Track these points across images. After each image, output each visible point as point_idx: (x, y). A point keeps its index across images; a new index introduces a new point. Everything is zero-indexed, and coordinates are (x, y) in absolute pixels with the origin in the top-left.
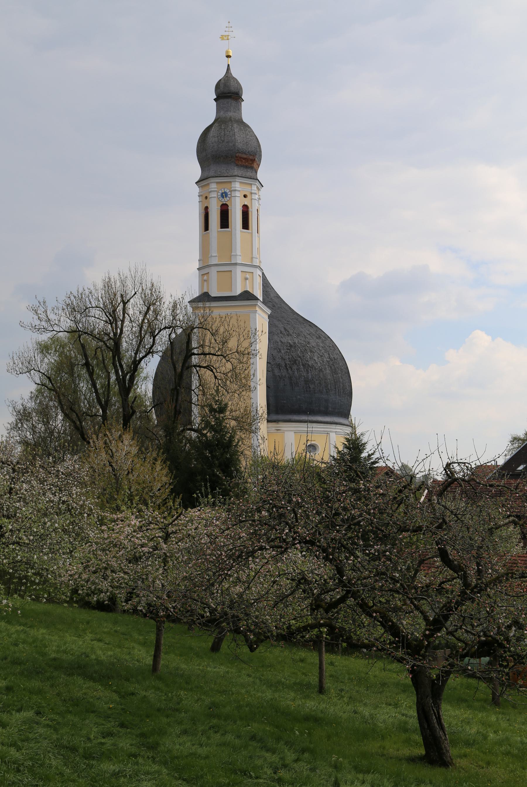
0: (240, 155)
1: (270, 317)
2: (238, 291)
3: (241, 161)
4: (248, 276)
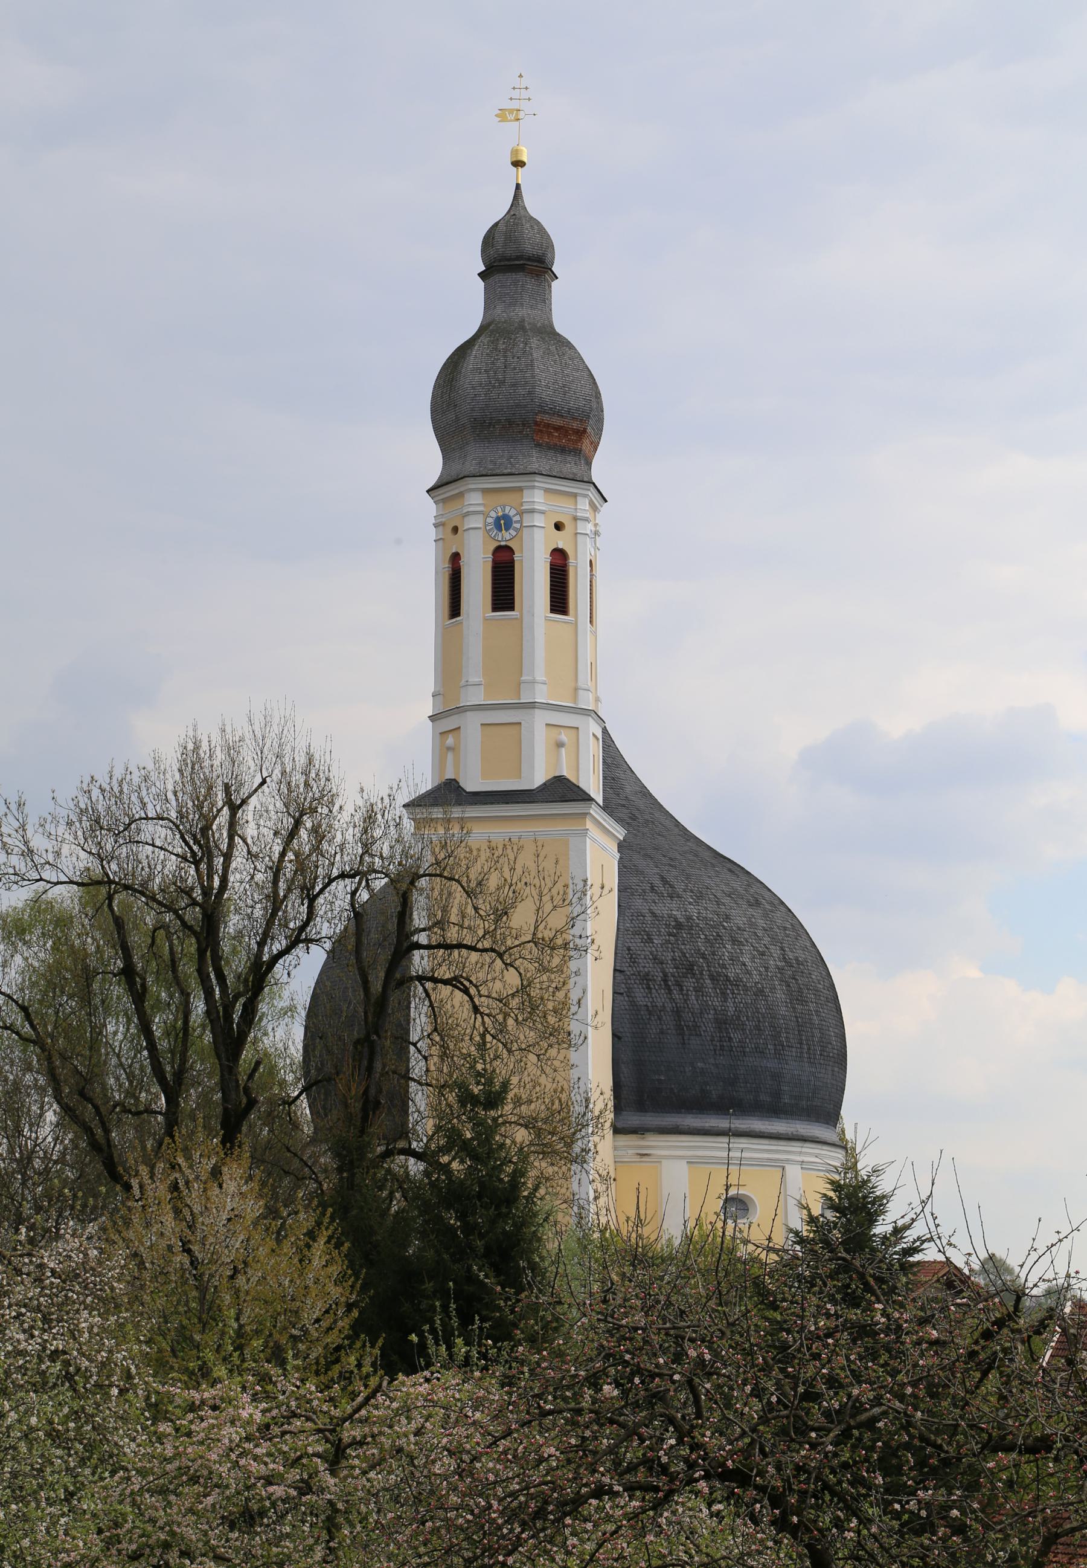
0: (546, 418)
1: (621, 846)
2: (539, 778)
3: (550, 434)
4: (564, 737)
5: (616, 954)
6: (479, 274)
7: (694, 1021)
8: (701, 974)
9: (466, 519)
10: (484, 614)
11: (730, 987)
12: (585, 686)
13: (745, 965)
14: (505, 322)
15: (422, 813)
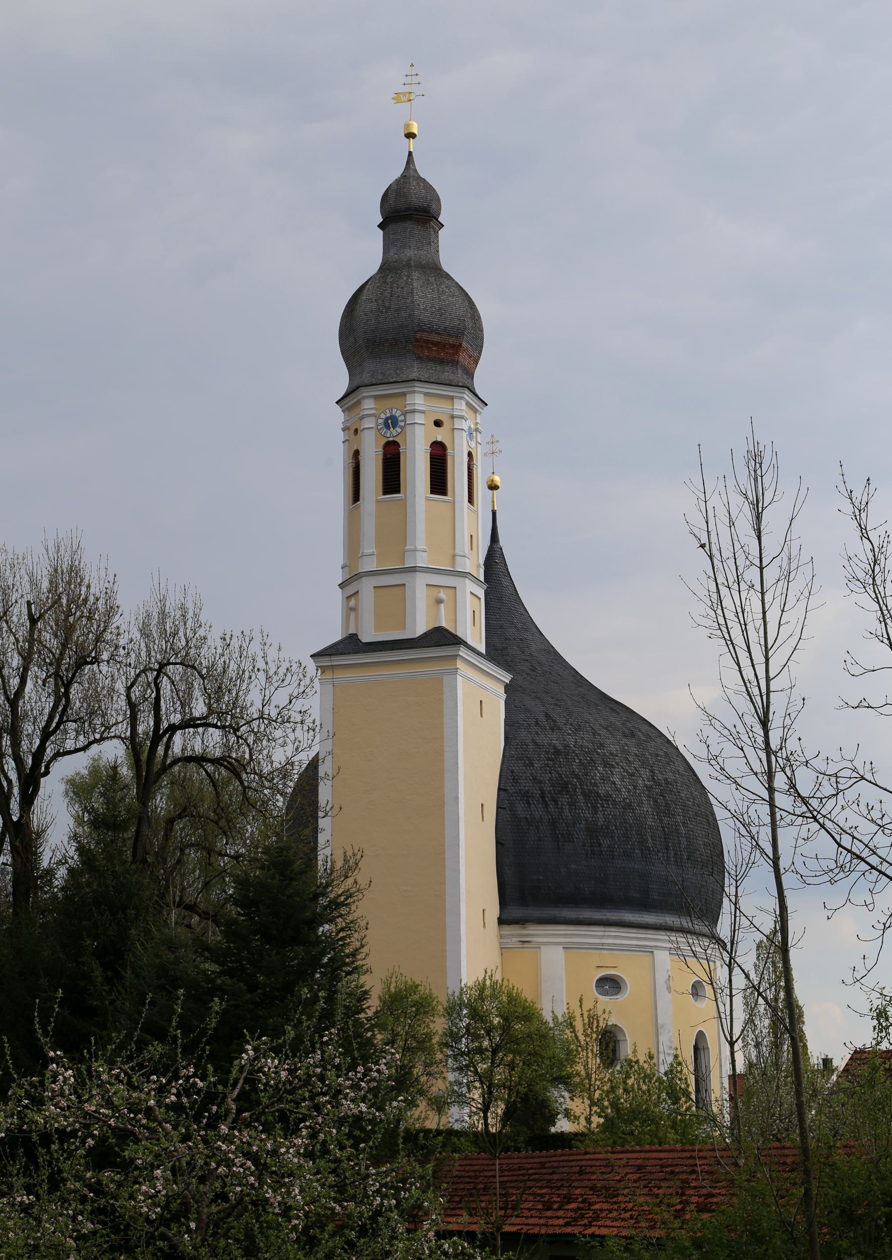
0: (425, 336)
1: (508, 688)
2: (420, 628)
3: (429, 349)
4: (442, 595)
5: (501, 776)
6: (378, 226)
7: (568, 830)
8: (575, 791)
9: (362, 421)
10: (376, 497)
11: (600, 802)
12: (461, 553)
13: (615, 784)
14: (396, 262)
15: (326, 661)
